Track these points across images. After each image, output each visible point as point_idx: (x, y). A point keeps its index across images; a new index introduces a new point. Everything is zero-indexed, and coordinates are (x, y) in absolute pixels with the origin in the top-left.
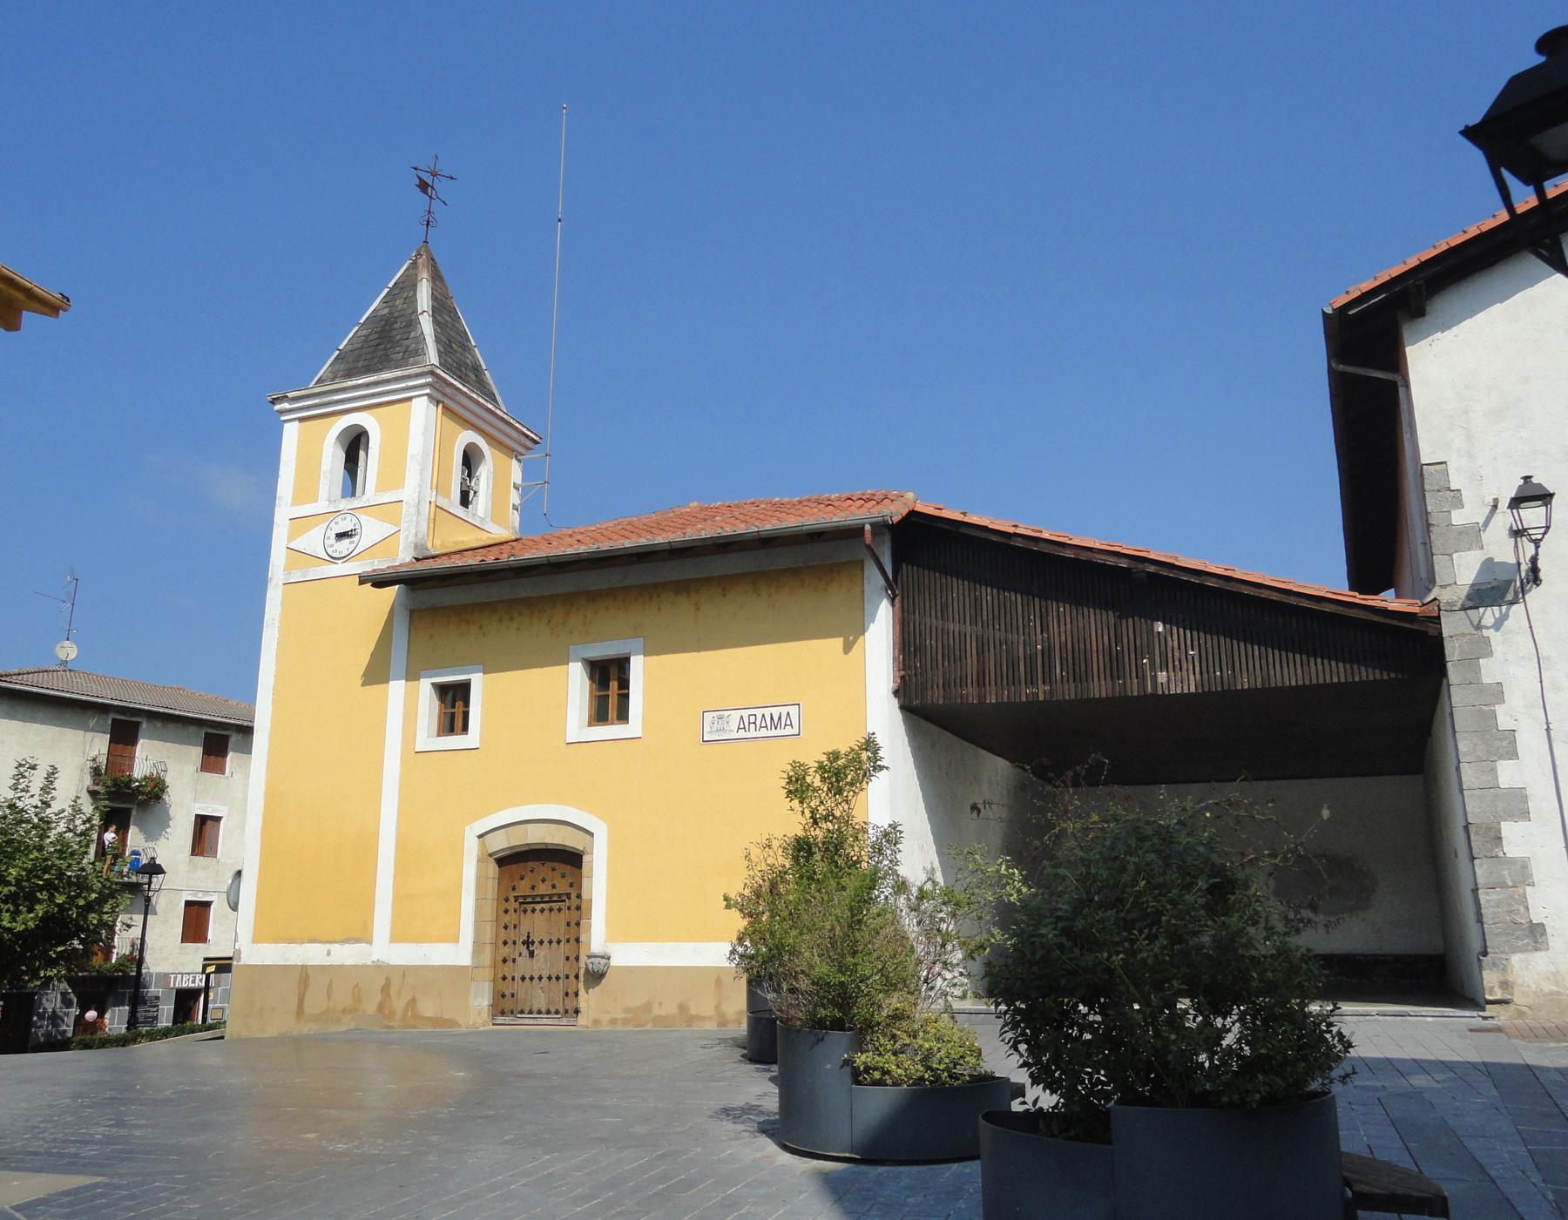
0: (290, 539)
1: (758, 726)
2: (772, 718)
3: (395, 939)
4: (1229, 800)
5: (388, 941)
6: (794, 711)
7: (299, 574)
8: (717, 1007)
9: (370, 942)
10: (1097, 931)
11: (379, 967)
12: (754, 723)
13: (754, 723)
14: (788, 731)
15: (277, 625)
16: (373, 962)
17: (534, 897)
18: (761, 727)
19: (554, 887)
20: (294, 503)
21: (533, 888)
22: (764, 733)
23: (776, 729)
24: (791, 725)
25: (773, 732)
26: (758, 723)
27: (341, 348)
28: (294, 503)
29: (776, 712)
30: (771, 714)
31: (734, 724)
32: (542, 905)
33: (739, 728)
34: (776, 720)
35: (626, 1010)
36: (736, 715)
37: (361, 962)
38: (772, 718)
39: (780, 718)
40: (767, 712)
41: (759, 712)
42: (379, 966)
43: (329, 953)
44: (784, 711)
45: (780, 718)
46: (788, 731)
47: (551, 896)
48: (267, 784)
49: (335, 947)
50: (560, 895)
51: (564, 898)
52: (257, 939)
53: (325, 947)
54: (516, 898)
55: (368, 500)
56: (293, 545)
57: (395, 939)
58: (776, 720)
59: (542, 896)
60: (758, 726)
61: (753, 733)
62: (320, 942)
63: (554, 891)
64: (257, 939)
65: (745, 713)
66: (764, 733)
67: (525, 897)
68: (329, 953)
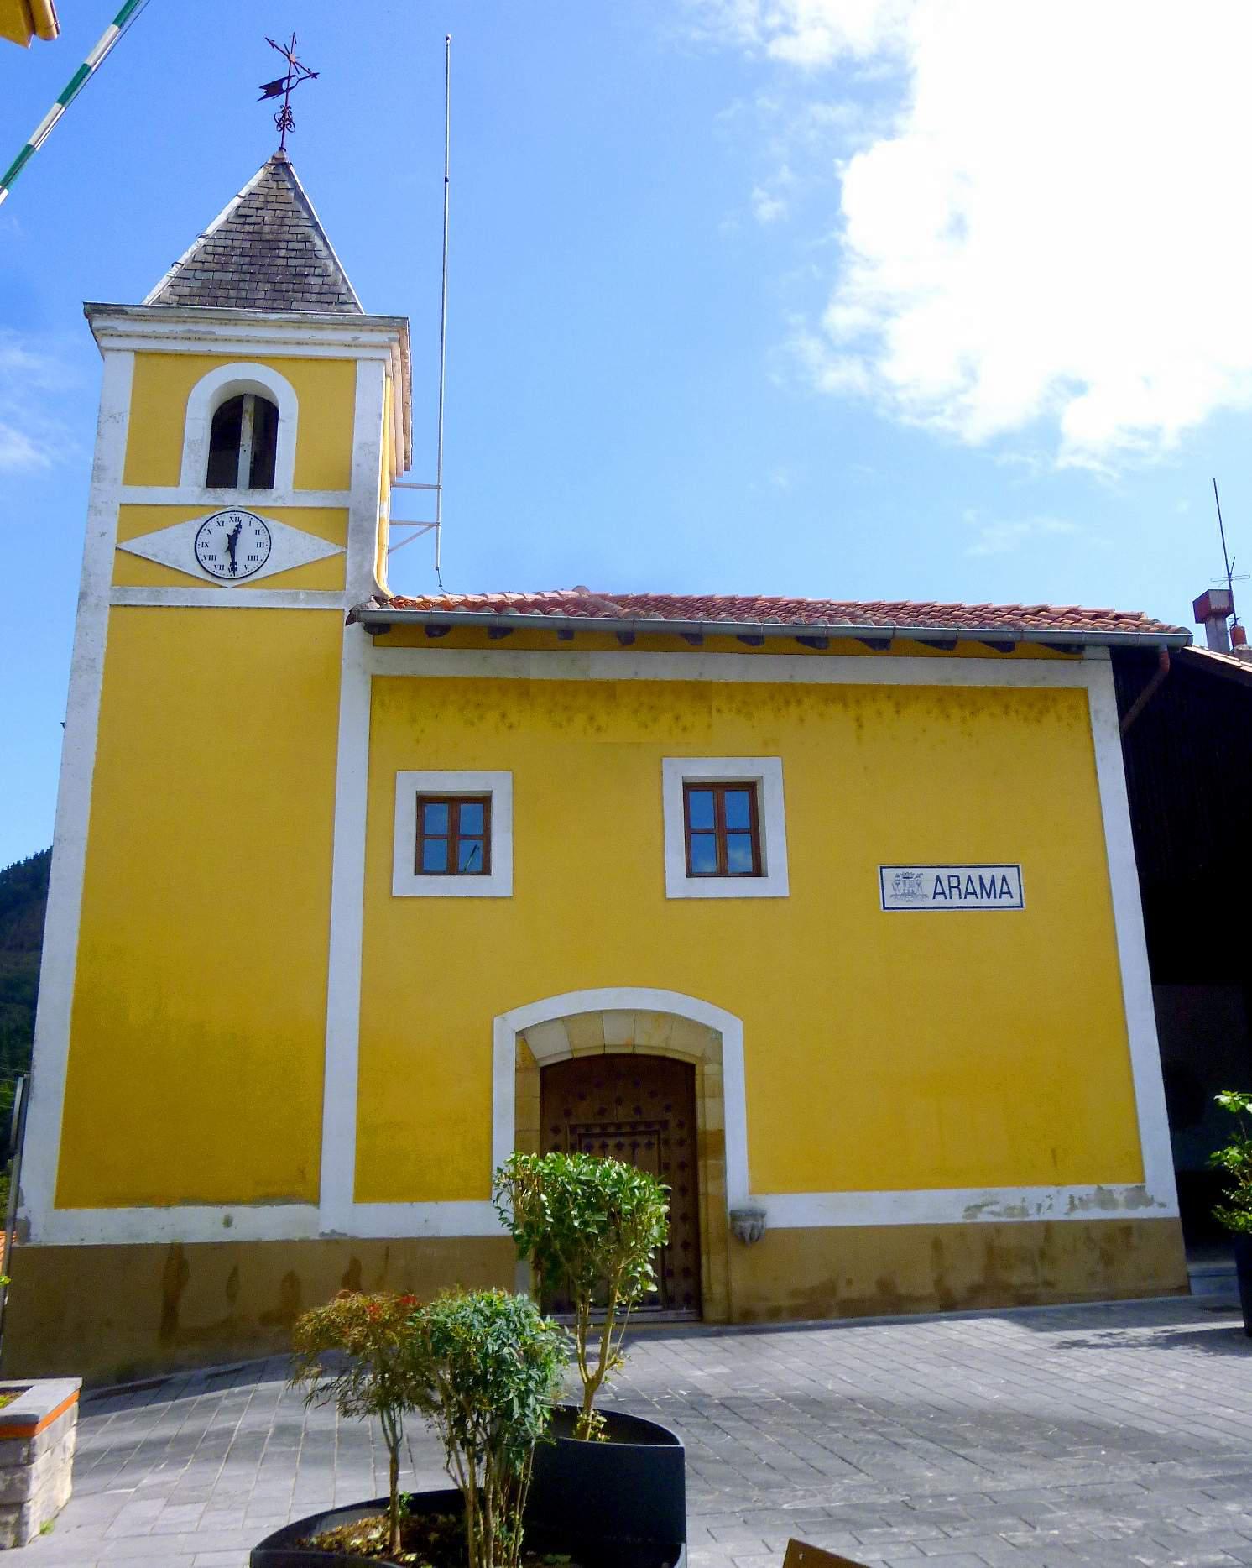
0: (119, 541)
1: (998, 892)
2: (982, 883)
3: (365, 1192)
4: (44, 1471)
5: (351, 1200)
6: (1011, 874)
7: (145, 594)
8: (938, 1282)
9: (315, 1201)
10: (1100, 1466)
11: (334, 1242)
12: (957, 887)
13: (957, 887)
14: (1006, 900)
15: (101, 669)
16: (323, 1234)
17: (604, 1127)
18: (1002, 893)
19: (638, 1110)
20: (128, 480)
21: (602, 1112)
22: (971, 901)
23: (989, 897)
24: (1009, 892)
25: (985, 902)
26: (963, 887)
27: (182, 261)
28: (128, 480)
29: (987, 874)
30: (993, 877)
31: (929, 887)
32: (618, 1139)
33: (935, 893)
34: (988, 884)
35: (794, 1293)
36: (932, 874)
37: (297, 1235)
38: (982, 883)
39: (993, 882)
40: (975, 874)
41: (963, 874)
42: (336, 1241)
43: (228, 1222)
44: (998, 873)
45: (993, 882)
46: (1006, 900)
47: (634, 1125)
48: (83, 932)
49: (241, 1213)
50: (649, 1124)
51: (657, 1127)
52: (66, 1198)
53: (221, 1212)
54: (573, 1129)
55: (280, 497)
56: (124, 546)
57: (365, 1192)
58: (988, 884)
59: (619, 1126)
60: (998, 892)
61: (956, 901)
62: (206, 1202)
63: (638, 1118)
64: (66, 1198)
65: (944, 874)
66: (971, 901)
67: (588, 1127)
68: (228, 1222)
